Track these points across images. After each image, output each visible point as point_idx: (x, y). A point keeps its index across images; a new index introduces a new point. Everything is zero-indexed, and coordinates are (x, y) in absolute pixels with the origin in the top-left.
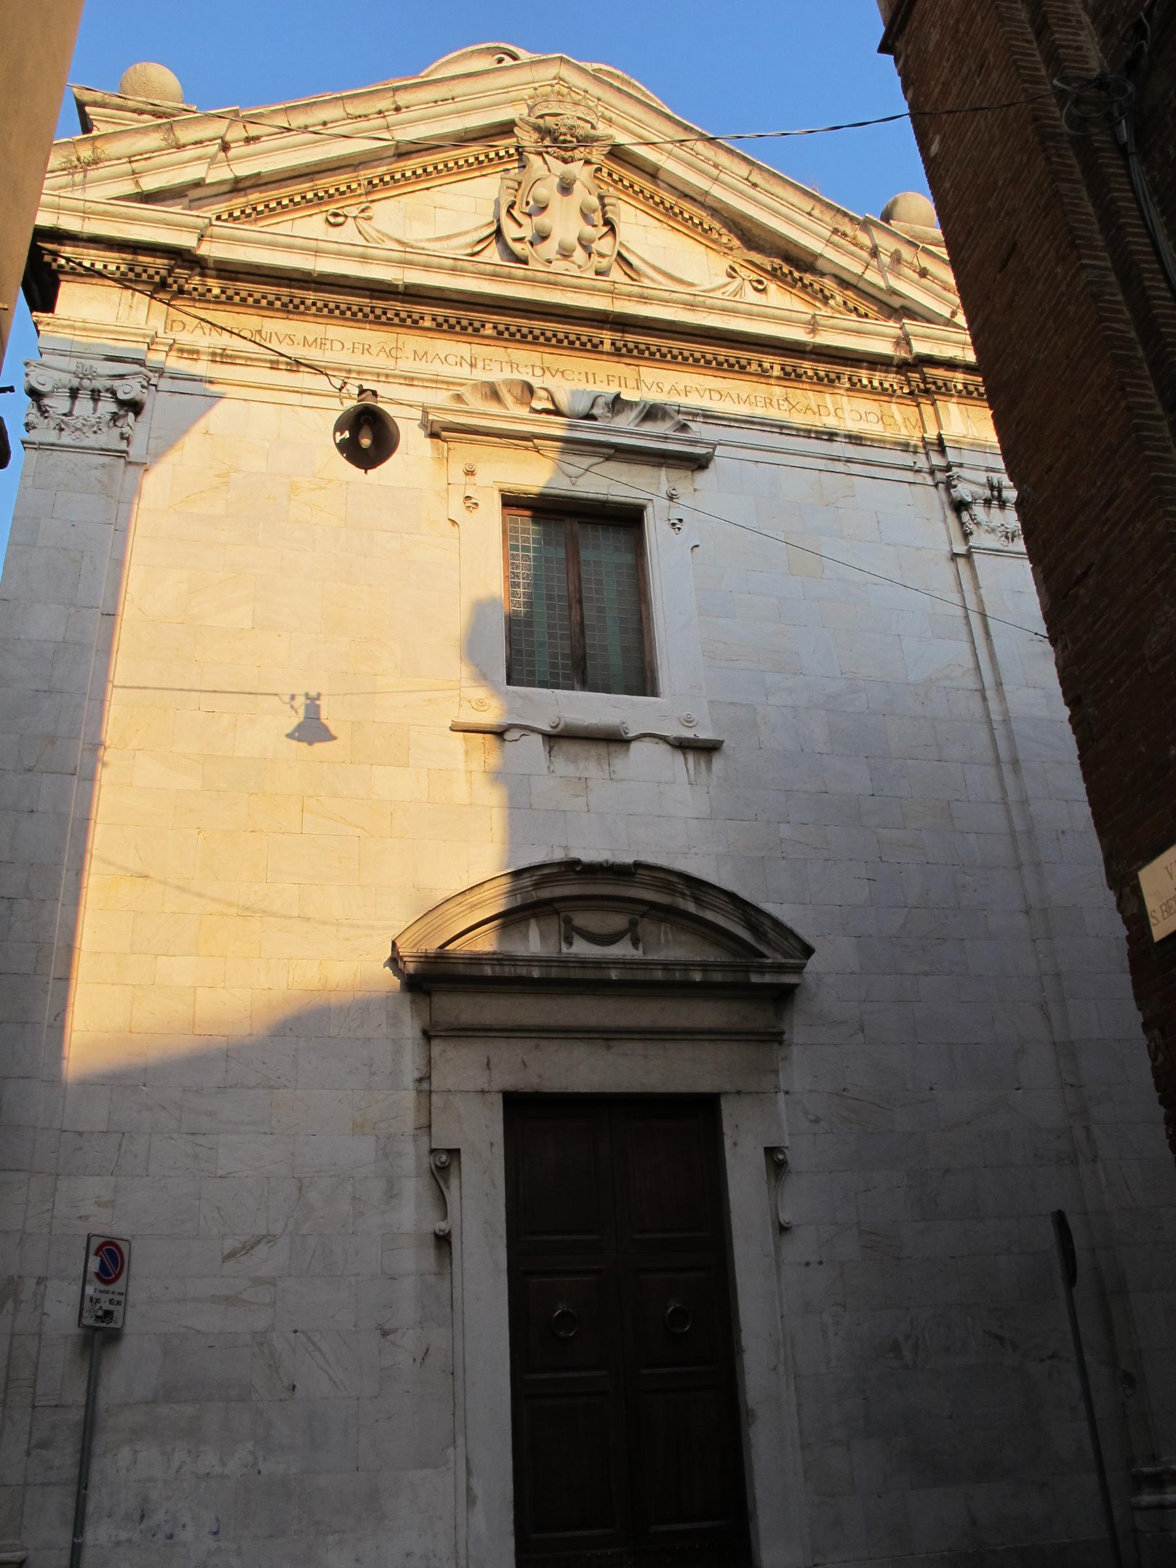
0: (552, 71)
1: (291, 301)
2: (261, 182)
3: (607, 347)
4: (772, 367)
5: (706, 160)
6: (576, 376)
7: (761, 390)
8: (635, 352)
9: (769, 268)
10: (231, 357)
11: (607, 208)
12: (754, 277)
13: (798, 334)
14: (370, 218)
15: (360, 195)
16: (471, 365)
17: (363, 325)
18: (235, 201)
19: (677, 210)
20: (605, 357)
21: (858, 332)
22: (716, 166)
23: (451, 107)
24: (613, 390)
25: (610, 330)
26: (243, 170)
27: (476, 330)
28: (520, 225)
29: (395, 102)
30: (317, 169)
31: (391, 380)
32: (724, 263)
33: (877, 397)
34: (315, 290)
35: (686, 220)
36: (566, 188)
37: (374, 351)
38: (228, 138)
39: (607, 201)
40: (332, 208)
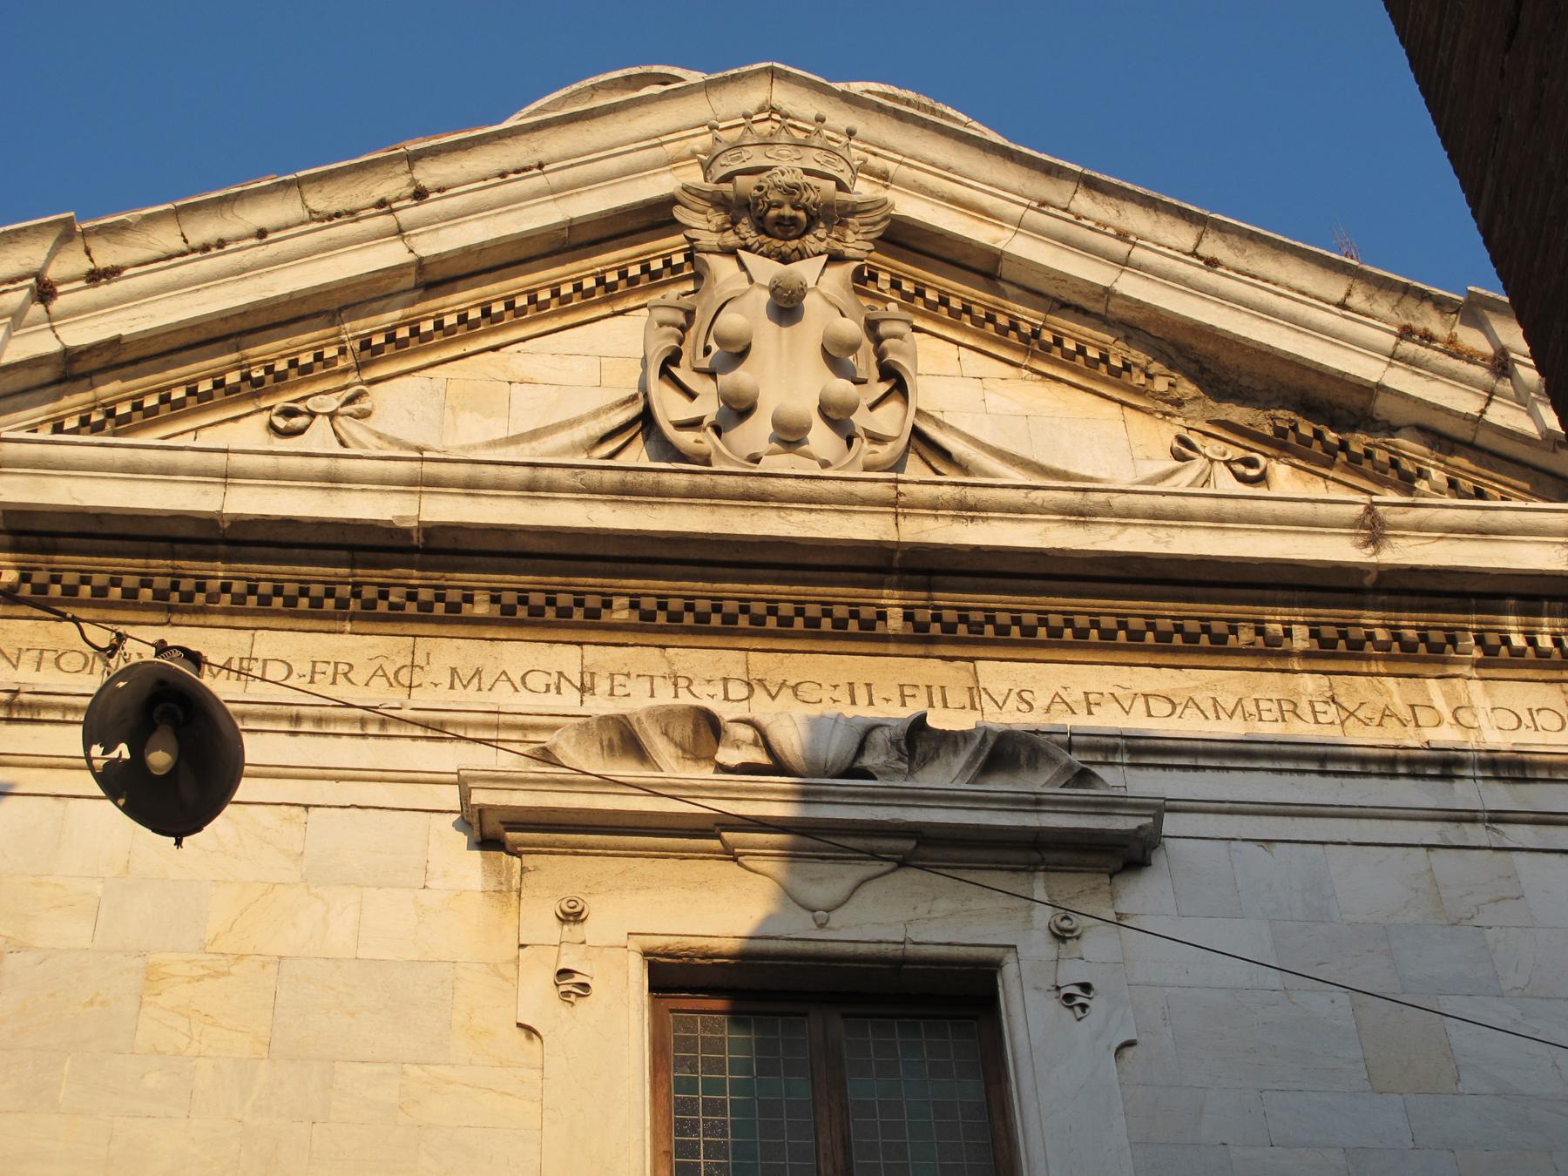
0: (752, 97)
1: (175, 587)
2: (125, 357)
3: (895, 622)
4: (1288, 633)
5: (1100, 227)
6: (826, 694)
7: (1270, 685)
8: (962, 630)
9: (1269, 432)
10: (31, 706)
11: (886, 344)
12: (1235, 453)
13: (1341, 550)
14: (365, 414)
15: (345, 371)
16: (583, 689)
17: (337, 625)
18: (67, 401)
19: (1047, 337)
20: (892, 648)
21: (1482, 532)
22: (1122, 236)
23: (538, 182)
24: (900, 713)
25: (898, 587)
26: (80, 334)
27: (593, 614)
28: (692, 396)
29: (414, 182)
30: (247, 325)
31: (392, 731)
32: (1163, 434)
33: (1554, 675)
34: (227, 559)
35: (1070, 355)
36: (786, 307)
37: (359, 676)
38: (52, 274)
39: (884, 329)
40: (281, 401)
